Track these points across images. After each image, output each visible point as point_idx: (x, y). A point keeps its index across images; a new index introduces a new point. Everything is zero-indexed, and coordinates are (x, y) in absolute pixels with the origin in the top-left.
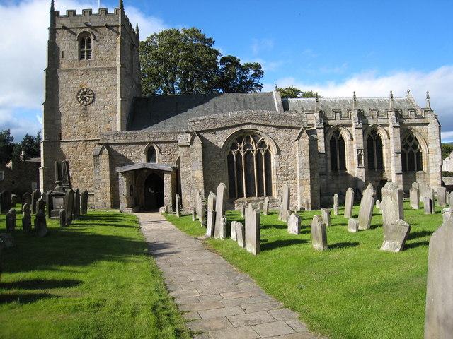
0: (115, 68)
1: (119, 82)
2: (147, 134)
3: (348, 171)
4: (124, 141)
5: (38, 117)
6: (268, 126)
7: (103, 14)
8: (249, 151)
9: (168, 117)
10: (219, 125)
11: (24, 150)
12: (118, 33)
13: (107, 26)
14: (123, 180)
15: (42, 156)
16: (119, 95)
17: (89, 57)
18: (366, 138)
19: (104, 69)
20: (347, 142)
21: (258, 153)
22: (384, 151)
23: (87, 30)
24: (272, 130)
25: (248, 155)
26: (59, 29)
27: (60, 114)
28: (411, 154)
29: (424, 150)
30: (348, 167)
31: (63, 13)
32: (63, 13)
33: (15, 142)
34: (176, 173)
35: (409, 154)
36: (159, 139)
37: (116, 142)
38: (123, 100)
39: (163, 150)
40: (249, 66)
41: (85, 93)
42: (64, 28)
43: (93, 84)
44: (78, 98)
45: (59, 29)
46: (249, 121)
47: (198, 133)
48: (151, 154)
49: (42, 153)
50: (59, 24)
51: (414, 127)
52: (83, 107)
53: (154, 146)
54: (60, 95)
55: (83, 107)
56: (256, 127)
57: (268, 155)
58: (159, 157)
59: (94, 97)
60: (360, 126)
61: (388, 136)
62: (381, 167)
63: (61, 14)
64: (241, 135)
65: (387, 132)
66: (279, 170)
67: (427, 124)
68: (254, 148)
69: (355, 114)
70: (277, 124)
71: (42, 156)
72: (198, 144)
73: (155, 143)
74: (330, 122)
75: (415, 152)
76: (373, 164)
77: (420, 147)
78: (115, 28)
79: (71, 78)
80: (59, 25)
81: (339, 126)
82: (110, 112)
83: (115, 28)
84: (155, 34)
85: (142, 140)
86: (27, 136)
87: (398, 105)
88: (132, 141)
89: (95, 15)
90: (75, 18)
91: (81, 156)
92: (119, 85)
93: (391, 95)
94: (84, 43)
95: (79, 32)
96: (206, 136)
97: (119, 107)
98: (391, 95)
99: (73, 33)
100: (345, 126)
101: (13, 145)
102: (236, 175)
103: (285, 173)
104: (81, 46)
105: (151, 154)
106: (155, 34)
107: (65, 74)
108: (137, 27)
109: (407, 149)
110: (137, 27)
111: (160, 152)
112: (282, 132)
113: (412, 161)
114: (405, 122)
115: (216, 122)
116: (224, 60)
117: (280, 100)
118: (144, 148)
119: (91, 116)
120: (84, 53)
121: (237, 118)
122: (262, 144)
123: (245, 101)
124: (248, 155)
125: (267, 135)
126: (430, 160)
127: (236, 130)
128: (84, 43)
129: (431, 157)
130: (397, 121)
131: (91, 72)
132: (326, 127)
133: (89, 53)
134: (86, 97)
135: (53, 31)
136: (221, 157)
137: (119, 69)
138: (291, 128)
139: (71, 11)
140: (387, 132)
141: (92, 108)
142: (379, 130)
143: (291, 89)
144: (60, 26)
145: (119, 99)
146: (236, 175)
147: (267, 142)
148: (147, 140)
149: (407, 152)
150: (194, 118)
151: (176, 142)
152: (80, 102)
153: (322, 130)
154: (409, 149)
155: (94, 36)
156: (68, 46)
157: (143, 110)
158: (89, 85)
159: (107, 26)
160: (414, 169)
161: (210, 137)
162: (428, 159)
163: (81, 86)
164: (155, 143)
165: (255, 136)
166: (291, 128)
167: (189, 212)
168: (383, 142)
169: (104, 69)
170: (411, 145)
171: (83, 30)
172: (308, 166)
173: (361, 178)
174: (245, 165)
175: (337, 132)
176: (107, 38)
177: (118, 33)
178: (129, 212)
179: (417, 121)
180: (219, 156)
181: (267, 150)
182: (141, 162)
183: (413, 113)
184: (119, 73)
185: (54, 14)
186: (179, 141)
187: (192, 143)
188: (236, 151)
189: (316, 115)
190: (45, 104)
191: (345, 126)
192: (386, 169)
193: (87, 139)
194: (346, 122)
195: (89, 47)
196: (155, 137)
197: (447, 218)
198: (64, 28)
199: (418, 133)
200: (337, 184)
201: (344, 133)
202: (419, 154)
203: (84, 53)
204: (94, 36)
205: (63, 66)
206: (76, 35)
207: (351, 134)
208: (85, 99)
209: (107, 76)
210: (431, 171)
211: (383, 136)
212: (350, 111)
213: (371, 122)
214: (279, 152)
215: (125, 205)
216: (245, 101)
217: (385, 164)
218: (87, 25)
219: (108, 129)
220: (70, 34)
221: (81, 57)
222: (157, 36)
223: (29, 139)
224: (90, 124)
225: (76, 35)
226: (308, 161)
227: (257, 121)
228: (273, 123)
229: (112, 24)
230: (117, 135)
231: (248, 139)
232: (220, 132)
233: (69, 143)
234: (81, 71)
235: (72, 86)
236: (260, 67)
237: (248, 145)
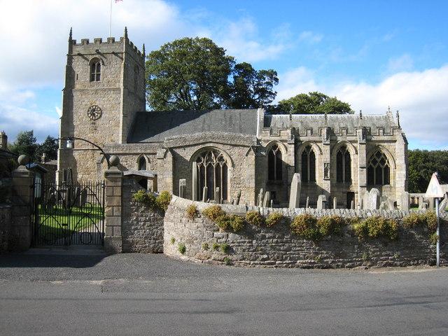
0: (119, 89)
1: (122, 102)
2: (138, 148)
3: (317, 183)
4: (121, 152)
5: (57, 108)
7: (111, 42)
9: (163, 131)
10: (187, 143)
11: (46, 152)
12: (122, 59)
13: (113, 53)
15: (58, 159)
16: (121, 112)
17: (98, 79)
18: (335, 152)
19: (110, 90)
20: (317, 157)
21: (218, 165)
22: (353, 165)
23: (97, 56)
25: (210, 167)
26: (75, 55)
27: (73, 127)
28: (379, 169)
29: (391, 166)
30: (317, 179)
32: (79, 42)
33: (37, 143)
34: (155, 178)
36: (148, 151)
38: (125, 116)
39: (151, 160)
40: (264, 72)
41: (94, 110)
42: (79, 55)
43: (100, 103)
44: (88, 114)
45: (75, 55)
47: (171, 149)
48: (142, 164)
49: (58, 156)
50: (76, 50)
51: (383, 144)
53: (145, 156)
54: (74, 111)
56: (216, 145)
57: (225, 167)
58: (148, 165)
59: (101, 114)
60: (364, 141)
61: (356, 151)
62: (349, 180)
64: (205, 151)
65: (355, 148)
66: (233, 180)
67: (395, 141)
69: (324, 131)
71: (58, 159)
72: (170, 157)
73: (146, 154)
74: (302, 138)
75: (383, 167)
77: (388, 162)
78: (120, 55)
80: (75, 52)
81: (310, 141)
82: (113, 129)
83: (120, 55)
84: (169, 44)
85: (135, 152)
86: (49, 138)
87: (368, 125)
88: (127, 152)
89: (105, 43)
90: (88, 46)
91: (89, 163)
92: (122, 104)
93: (71, 32)
94: (95, 66)
95: (90, 58)
96: (178, 151)
97: (121, 122)
98: (71, 32)
99: (86, 59)
100: (315, 142)
101: (36, 146)
103: (237, 181)
105: (142, 164)
106: (169, 44)
107: (78, 93)
109: (374, 164)
111: (149, 162)
112: (236, 149)
113: (379, 175)
114: (373, 139)
115: (185, 140)
116: (239, 67)
117: (262, 117)
118: (136, 157)
119: (98, 129)
120: (94, 77)
121: (202, 138)
122: (221, 159)
123: (231, 118)
124: (210, 167)
125: (224, 151)
126: (397, 176)
127: (200, 147)
128: (95, 66)
129: (397, 172)
130: (327, 139)
131: (100, 92)
132: (297, 143)
133: (98, 75)
134: (94, 113)
135: (70, 58)
137: (122, 90)
138: (244, 146)
140: (355, 148)
141: (99, 122)
142: (348, 146)
143: (315, 94)
144: (76, 53)
145: (122, 115)
147: (225, 157)
148: (139, 151)
150: (169, 137)
152: (90, 117)
153: (293, 146)
155: (103, 62)
156: (82, 69)
157: (141, 126)
158: (97, 103)
159: (113, 53)
160: (381, 183)
161: (180, 152)
162: (394, 174)
164: (146, 154)
165: (215, 152)
166: (244, 146)
168: (352, 157)
169: (110, 90)
170: (379, 160)
171: (95, 56)
172: (254, 177)
173: (326, 189)
174: (207, 173)
175: (309, 147)
176: (114, 63)
177: (122, 59)
179: (386, 138)
180: (186, 167)
182: (133, 169)
183: (381, 131)
184: (122, 93)
185: (72, 43)
187: (165, 156)
189: (289, 131)
190: (62, 118)
191: (315, 142)
192: (353, 182)
194: (317, 138)
195: (99, 71)
196: (146, 149)
198: (79, 55)
199: (386, 149)
201: (315, 148)
202: (387, 169)
203: (94, 77)
204: (103, 62)
205: (78, 86)
206: (88, 60)
207: (320, 149)
208: (94, 115)
209: (112, 95)
210: (397, 186)
211: (352, 152)
212: (320, 129)
213: (340, 139)
214: (233, 165)
216: (231, 118)
217: (352, 178)
218: (98, 53)
219: (112, 140)
220: (83, 60)
221: (92, 79)
222: (171, 45)
223: (50, 141)
225: (88, 60)
226: (254, 173)
227: (217, 141)
229: (118, 51)
231: (210, 154)
232: (189, 148)
234: (92, 91)
235: (84, 103)
236: (276, 73)
237: (210, 159)
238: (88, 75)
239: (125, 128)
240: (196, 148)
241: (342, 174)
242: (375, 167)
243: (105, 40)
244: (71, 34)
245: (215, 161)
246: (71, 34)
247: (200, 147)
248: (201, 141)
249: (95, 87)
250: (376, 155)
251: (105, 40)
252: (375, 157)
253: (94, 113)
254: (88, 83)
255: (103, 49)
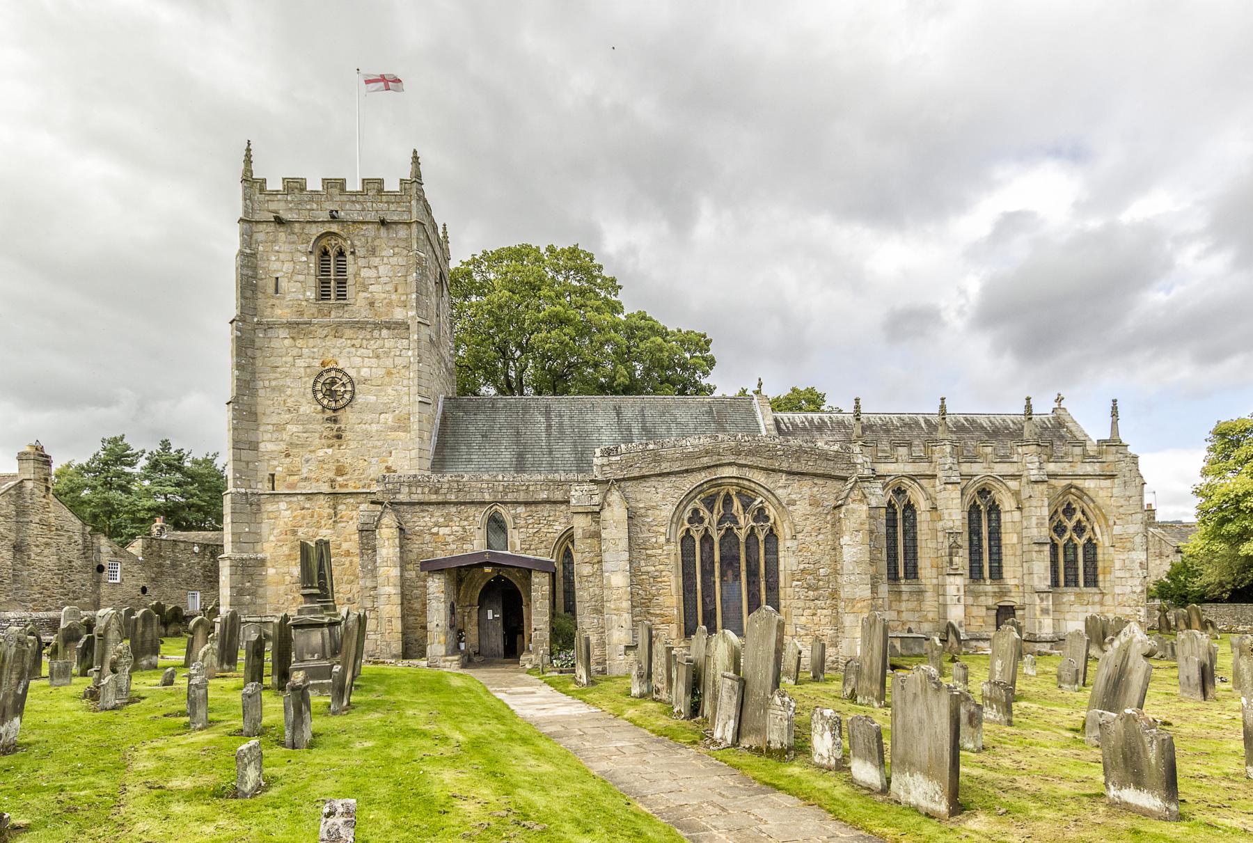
6: (774, 470)
8: (729, 529)
10: (665, 467)
14: (436, 586)
17: (342, 296)
18: (967, 508)
21: (752, 534)
23: (334, 228)
24: (782, 482)
31: (275, 184)
32: (275, 184)
35: (1084, 546)
37: (415, 498)
43: (355, 360)
44: (314, 392)
46: (732, 459)
52: (329, 414)
55: (329, 414)
56: (749, 474)
57: (772, 536)
63: (269, 187)
68: (742, 522)
70: (795, 467)
76: (981, 568)
79: (299, 343)
93: (248, 150)
98: (248, 150)
102: (699, 587)
104: (323, 269)
105: (496, 525)
108: (445, 228)
110: (445, 228)
122: (761, 515)
127: (702, 477)
133: (342, 283)
136: (668, 541)
139: (295, 180)
141: (349, 418)
146: (699, 587)
149: (1061, 542)
151: (567, 502)
154: (1067, 536)
156: (291, 266)
163: (323, 364)
167: (622, 672)
169: (378, 326)
170: (1070, 525)
172: (1100, 570)
178: (451, 666)
181: (1090, 540)
186: (573, 501)
188: (701, 528)
193: (338, 490)
195: (341, 270)
197: (75, 614)
200: (899, 612)
211: (1007, 503)
215: (442, 650)
219: (388, 469)
221: (324, 295)
224: (346, 454)
228: (785, 466)
230: (414, 482)
231: (728, 500)
233: (294, 499)
238: (312, 281)
239: (426, 426)
240: (689, 483)
241: (1077, 569)
242: (1061, 542)
243: (354, 185)
244: (248, 160)
245: (745, 522)
246: (248, 160)
247: (702, 477)
248: (706, 460)
249: (334, 316)
250: (1064, 512)
251: (354, 185)
252: (1062, 517)
253: (333, 392)
254: (310, 312)
255: (350, 212)
